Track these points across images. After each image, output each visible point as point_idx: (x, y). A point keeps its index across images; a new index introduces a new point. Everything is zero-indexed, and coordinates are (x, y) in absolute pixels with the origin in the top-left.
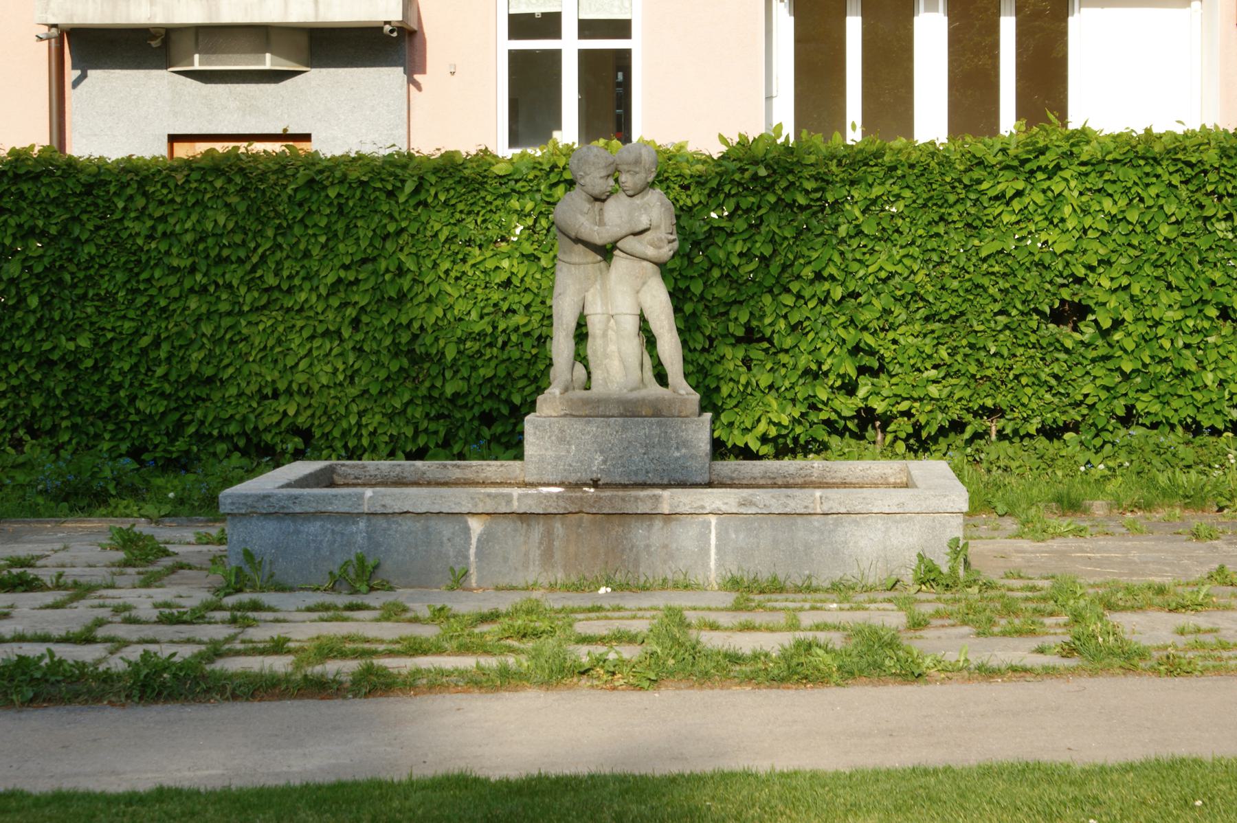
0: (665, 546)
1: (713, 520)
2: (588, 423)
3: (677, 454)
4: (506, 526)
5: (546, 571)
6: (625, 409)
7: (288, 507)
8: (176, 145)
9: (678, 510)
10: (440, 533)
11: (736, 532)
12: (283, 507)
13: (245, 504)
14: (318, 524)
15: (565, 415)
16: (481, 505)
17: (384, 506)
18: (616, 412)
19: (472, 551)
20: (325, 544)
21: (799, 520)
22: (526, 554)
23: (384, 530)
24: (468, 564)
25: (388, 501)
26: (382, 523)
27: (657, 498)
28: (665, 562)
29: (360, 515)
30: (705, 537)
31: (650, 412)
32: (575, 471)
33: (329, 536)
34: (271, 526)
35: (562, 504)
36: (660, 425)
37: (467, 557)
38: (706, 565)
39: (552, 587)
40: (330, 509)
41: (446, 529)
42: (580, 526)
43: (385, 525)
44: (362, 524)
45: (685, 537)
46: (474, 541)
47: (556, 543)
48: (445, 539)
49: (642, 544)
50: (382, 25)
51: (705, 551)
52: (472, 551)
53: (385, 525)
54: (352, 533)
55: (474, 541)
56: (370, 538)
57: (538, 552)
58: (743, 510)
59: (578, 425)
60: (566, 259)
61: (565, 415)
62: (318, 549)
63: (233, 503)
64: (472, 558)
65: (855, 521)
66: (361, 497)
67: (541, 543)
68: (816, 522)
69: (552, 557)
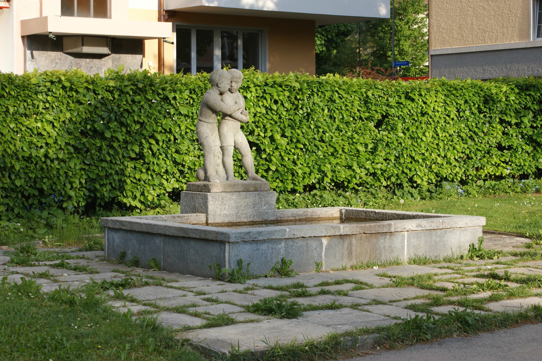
0: (390, 246)
1: (406, 233)
2: (232, 195)
3: (265, 208)
4: (335, 240)
5: (349, 261)
6: (244, 188)
7: (257, 238)
8: (157, 40)
9: (397, 230)
10: (312, 246)
11: (413, 238)
12: (255, 238)
13: (240, 237)
14: (266, 245)
15: (222, 192)
16: (329, 232)
17: (294, 235)
18: (241, 190)
19: (323, 253)
20: (269, 254)
21: (433, 232)
22: (342, 254)
23: (292, 246)
24: (321, 260)
25: (295, 232)
26: (291, 243)
27: (390, 225)
28: (390, 253)
29: (282, 239)
30: (403, 241)
31: (253, 190)
32: (228, 216)
33: (270, 250)
34: (248, 247)
35: (358, 230)
36: (259, 195)
37: (321, 257)
38: (403, 254)
39: (72, 252)
40: (273, 237)
41: (313, 244)
42: (361, 239)
43: (291, 244)
44: (283, 244)
45: (397, 241)
46: (324, 249)
47: (353, 248)
48: (314, 249)
49: (382, 246)
50: (48, 33)
51: (403, 247)
52: (323, 253)
53: (291, 244)
54: (279, 248)
55: (324, 249)
56: (286, 250)
57: (347, 252)
58: (417, 229)
59: (229, 196)
60: (207, 121)
61: (222, 192)
62: (266, 257)
63: (235, 237)
64: (323, 257)
65: (451, 232)
66: (285, 231)
67: (348, 248)
68: (439, 232)
69: (352, 254)
